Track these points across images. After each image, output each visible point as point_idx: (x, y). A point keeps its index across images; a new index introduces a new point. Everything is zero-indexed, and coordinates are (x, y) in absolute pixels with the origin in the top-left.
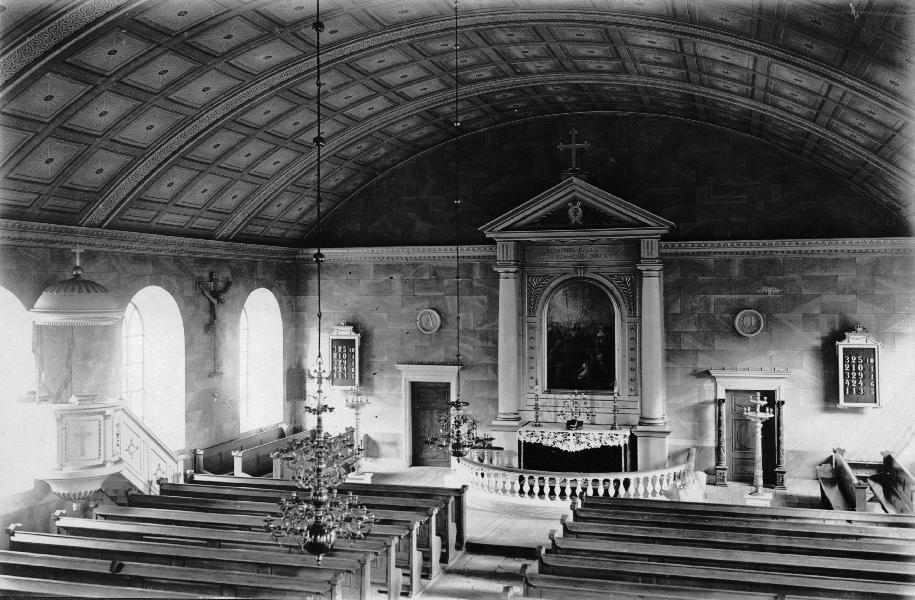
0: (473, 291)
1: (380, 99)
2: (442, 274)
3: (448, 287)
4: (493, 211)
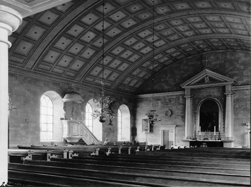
0: (179, 104)
1: (148, 47)
2: (171, 100)
3: (173, 104)
4: (184, 80)
